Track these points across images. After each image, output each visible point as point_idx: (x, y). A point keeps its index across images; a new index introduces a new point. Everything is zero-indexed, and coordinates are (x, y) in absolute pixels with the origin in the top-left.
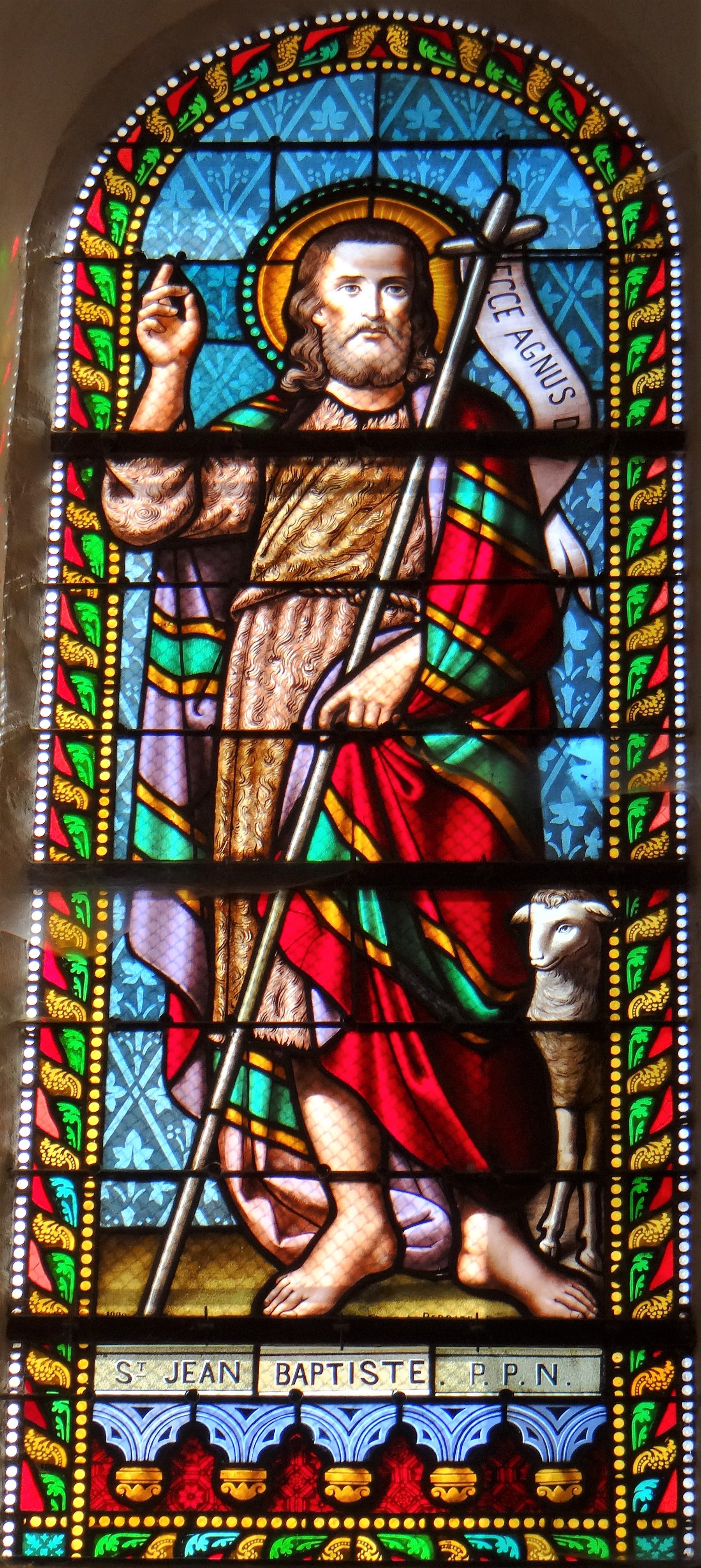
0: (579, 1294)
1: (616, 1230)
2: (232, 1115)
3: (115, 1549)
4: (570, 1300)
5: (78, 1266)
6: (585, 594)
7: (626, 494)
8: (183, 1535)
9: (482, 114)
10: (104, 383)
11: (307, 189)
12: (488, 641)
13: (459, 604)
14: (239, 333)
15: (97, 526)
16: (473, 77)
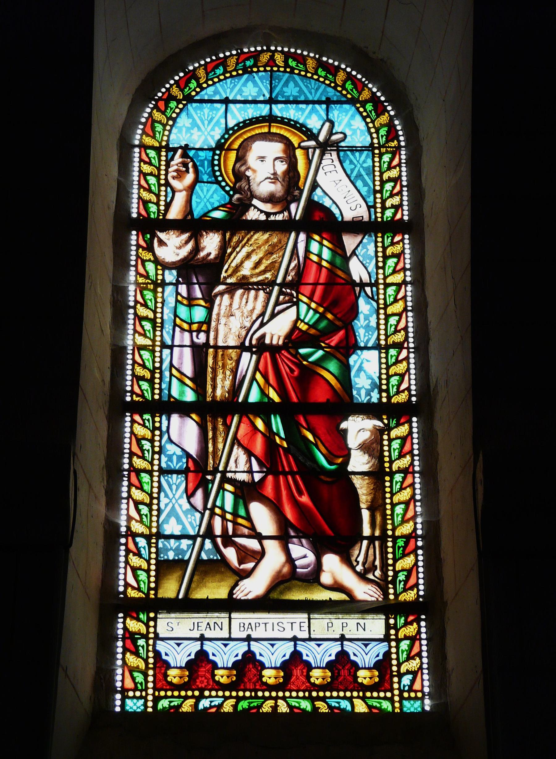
0: (375, 590)
1: (390, 562)
2: (217, 511)
3: (167, 706)
4: (372, 593)
5: (149, 577)
6: (368, 289)
7: (384, 249)
8: (198, 699)
9: (317, 90)
10: (154, 199)
11: (241, 120)
12: (327, 310)
13: (313, 293)
14: (213, 179)
15: (152, 259)
16: (313, 74)
